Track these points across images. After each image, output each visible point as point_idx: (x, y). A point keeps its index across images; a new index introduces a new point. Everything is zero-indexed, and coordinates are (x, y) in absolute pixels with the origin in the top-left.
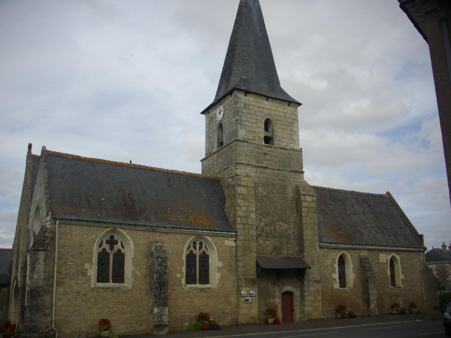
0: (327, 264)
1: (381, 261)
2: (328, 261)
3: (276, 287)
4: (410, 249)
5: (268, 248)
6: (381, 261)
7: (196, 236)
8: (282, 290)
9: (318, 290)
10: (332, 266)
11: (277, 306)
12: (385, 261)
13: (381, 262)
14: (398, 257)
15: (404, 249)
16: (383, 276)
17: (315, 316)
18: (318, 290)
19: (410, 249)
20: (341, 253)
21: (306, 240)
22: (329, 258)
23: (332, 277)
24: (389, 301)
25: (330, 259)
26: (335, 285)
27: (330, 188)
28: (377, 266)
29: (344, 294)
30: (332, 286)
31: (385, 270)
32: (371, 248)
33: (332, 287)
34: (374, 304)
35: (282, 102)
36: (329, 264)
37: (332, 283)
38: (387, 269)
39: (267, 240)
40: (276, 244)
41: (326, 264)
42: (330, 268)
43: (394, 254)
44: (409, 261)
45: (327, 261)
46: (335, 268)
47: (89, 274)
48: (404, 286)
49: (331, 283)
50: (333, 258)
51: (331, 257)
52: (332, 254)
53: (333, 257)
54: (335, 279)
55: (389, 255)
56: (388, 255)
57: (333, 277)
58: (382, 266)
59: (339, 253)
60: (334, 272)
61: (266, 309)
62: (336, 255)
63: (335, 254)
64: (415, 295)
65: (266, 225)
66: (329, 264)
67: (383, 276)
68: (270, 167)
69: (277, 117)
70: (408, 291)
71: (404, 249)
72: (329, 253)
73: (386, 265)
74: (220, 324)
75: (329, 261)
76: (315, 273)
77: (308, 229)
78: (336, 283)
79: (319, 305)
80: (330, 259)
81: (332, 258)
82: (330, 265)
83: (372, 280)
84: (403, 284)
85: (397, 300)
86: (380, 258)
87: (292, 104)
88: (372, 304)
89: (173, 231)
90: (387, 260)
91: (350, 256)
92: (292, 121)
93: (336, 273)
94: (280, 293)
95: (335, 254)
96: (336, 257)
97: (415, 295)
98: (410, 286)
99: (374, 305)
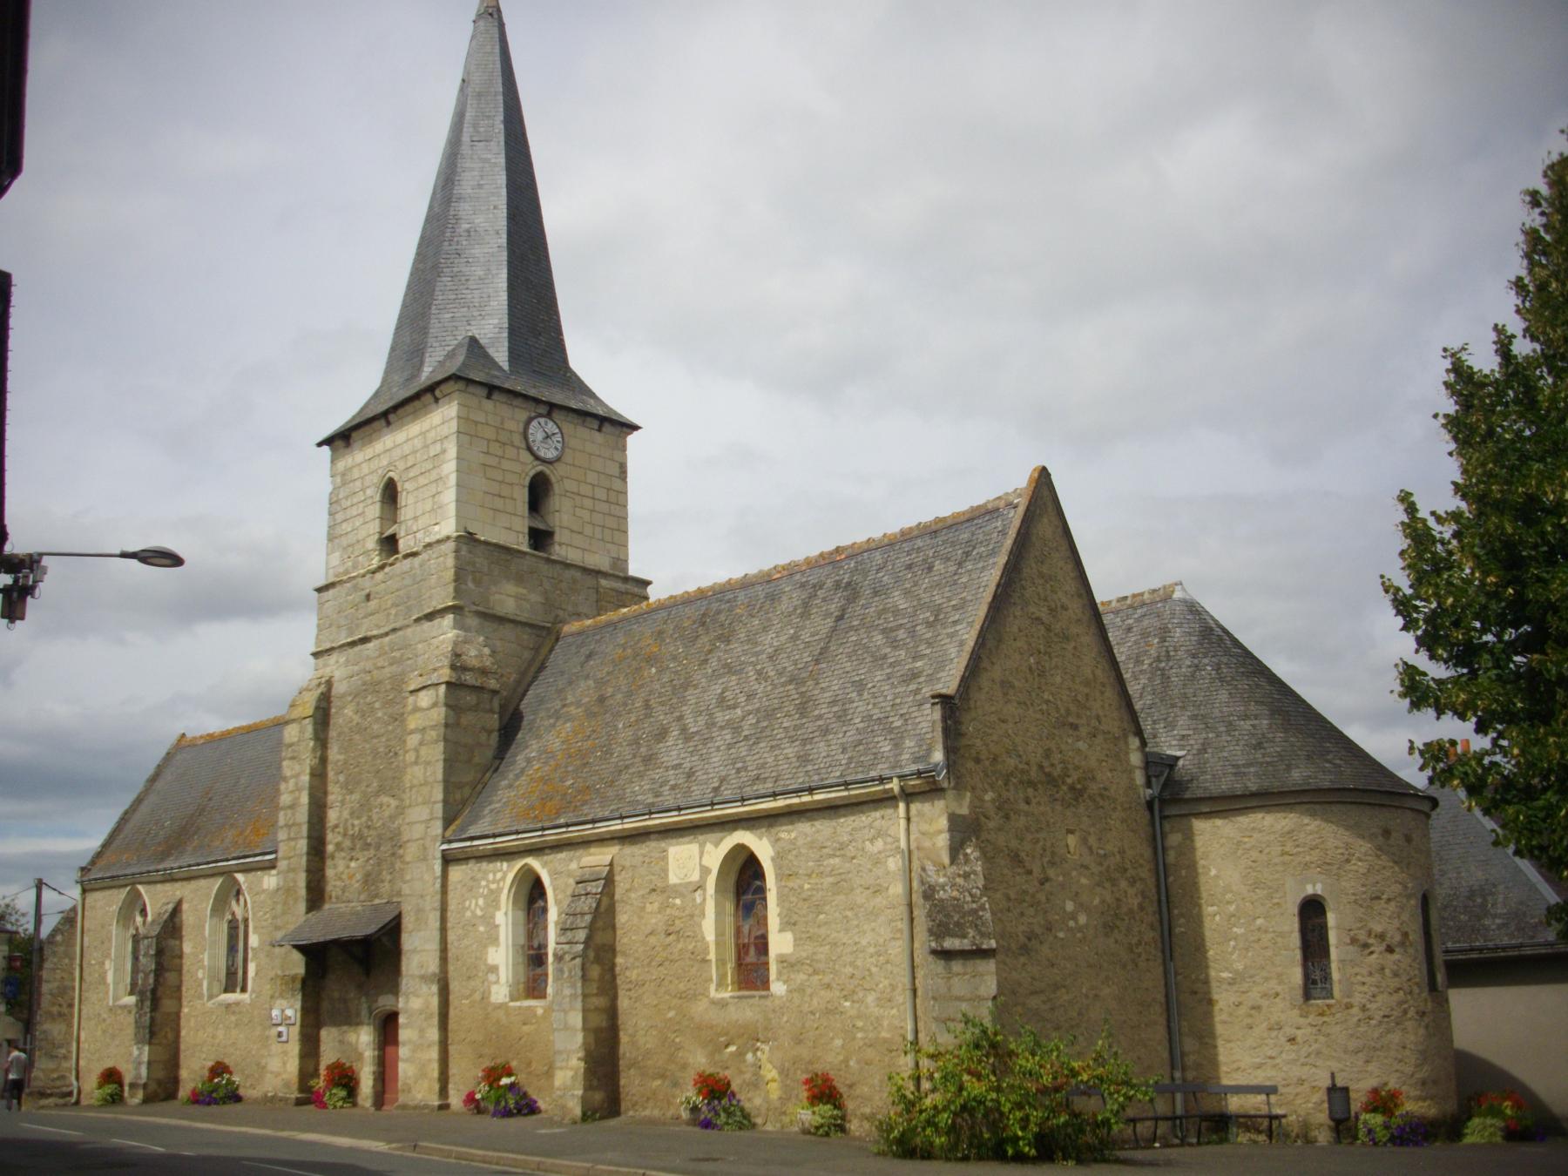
0: (473, 913)
1: (673, 879)
2: (477, 904)
3: (363, 999)
5: (354, 881)
6: (673, 879)
7: (128, 888)
8: (374, 1007)
9: (427, 1007)
10: (488, 919)
11: (360, 1056)
12: (695, 877)
13: (675, 885)
15: (780, 803)
16: (680, 946)
17: (419, 1096)
18: (427, 1007)
19: (818, 797)
20: (519, 864)
21: (408, 841)
22: (481, 890)
23: (486, 960)
24: (704, 1060)
25: (482, 895)
26: (494, 988)
27: (941, 515)
29: (525, 1024)
30: (483, 993)
31: (692, 916)
33: (485, 997)
34: (571, 1069)
35: (367, 429)
37: (486, 983)
39: (351, 859)
40: (369, 868)
41: (468, 914)
42: (482, 929)
45: (474, 902)
46: (497, 926)
48: (790, 991)
49: (483, 982)
50: (491, 891)
52: (491, 877)
53: (493, 886)
54: (494, 969)
55: (717, 845)
56: (709, 847)
57: (490, 961)
58: (678, 901)
59: (513, 868)
60: (495, 941)
62: (503, 878)
63: (499, 875)
64: (859, 1035)
65: (352, 814)
66: (479, 913)
67: (680, 946)
68: (375, 632)
70: (813, 1013)
72: (480, 875)
73: (699, 892)
75: (481, 902)
76: (424, 951)
77: (417, 805)
78: (497, 982)
79: (430, 1060)
80: (482, 895)
82: (481, 917)
83: (566, 969)
86: (670, 868)
87: (392, 417)
88: (561, 1068)
89: (97, 886)
90: (705, 871)
91: (550, 875)
94: (371, 1014)
95: (499, 875)
96: (501, 884)
97: (859, 1035)
98: (828, 986)
99: (570, 1073)
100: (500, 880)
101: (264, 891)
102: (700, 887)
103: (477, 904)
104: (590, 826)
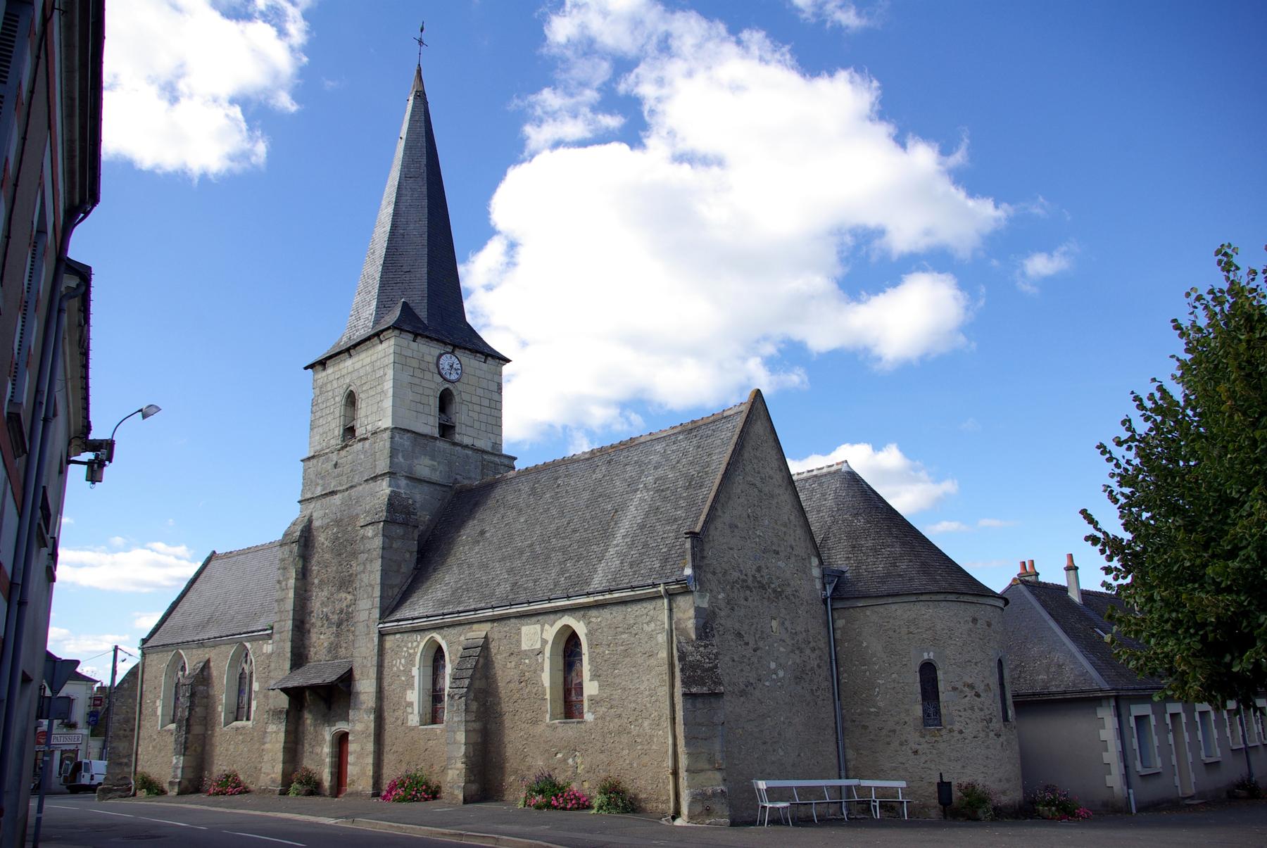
2: (400, 663)
4: (616, 595)
6: (524, 647)
10: (408, 672)
12: (538, 646)
13: (525, 651)
14: (580, 629)
19: (616, 595)
22: (403, 654)
25: (404, 657)
26: (410, 717)
28: (513, 663)
32: (491, 614)
36: (402, 668)
38: (542, 670)
41: (395, 669)
43: (568, 620)
44: (624, 633)
45: (398, 661)
47: (596, 684)
51: (407, 651)
52: (410, 645)
54: (410, 704)
56: (547, 626)
57: (408, 700)
58: (527, 661)
60: (412, 686)
61: (980, 780)
63: (415, 644)
69: (430, 352)
71: (591, 599)
74: (252, 787)
75: (403, 661)
76: (366, 693)
80: (404, 657)
81: (408, 653)
84: (593, 713)
85: (570, 761)
88: (451, 769)
90: (544, 642)
92: (430, 352)
93: (413, 690)
100: (416, 647)
101: (263, 654)
102: (540, 652)
103: (400, 663)
104: (473, 613)
